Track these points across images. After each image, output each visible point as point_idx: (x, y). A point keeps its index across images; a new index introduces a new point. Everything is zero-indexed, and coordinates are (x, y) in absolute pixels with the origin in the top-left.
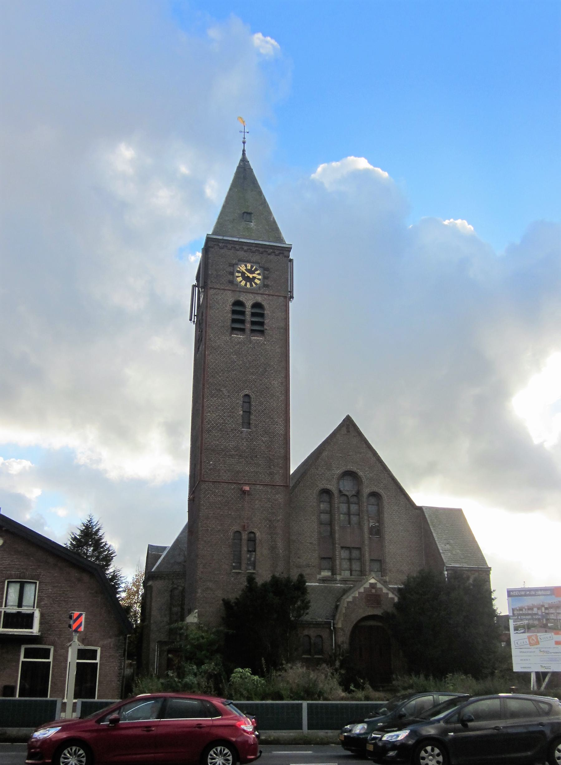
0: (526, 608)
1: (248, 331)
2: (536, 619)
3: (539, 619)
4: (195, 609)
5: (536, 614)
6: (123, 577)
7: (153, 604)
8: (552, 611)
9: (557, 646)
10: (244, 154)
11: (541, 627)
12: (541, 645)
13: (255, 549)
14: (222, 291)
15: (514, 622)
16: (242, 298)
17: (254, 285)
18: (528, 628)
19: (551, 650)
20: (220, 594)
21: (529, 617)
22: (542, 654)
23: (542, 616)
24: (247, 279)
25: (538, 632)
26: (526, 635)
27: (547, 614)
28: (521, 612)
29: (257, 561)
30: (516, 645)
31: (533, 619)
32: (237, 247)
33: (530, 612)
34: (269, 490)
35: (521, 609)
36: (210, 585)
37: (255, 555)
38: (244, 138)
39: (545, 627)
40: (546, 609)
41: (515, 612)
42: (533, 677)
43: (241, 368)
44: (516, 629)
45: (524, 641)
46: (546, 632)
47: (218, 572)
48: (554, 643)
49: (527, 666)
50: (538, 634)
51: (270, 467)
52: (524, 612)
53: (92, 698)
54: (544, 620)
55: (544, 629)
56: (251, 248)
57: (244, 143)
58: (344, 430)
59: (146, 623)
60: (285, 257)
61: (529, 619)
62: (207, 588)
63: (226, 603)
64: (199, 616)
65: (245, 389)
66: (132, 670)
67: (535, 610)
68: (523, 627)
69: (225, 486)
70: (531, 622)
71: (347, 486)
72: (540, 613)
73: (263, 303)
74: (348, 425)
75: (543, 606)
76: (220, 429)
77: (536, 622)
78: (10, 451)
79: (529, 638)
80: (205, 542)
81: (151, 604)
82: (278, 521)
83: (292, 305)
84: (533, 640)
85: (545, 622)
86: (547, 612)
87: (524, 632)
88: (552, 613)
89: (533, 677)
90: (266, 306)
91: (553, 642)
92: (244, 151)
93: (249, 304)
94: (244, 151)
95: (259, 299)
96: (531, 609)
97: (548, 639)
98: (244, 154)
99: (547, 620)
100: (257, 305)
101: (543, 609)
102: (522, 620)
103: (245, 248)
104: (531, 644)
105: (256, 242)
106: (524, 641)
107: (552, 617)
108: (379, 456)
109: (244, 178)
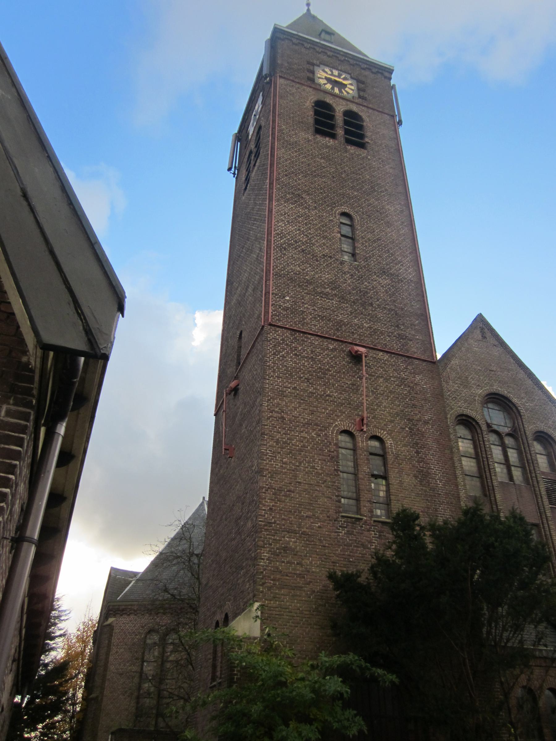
4: (255, 598)
6: (65, 611)
7: (111, 658)
13: (386, 470)
14: (298, 86)
17: (345, 93)
20: (317, 570)
29: (392, 497)
34: (403, 366)
36: (292, 541)
37: (388, 485)
43: (333, 177)
47: (310, 513)
51: (397, 326)
58: (478, 334)
59: (93, 696)
60: (385, 77)
62: (285, 549)
63: (344, 583)
64: (265, 620)
65: (342, 205)
66: (388, 556)
69: (317, 342)
71: (497, 418)
74: (482, 329)
76: (303, 251)
80: (277, 442)
81: (107, 659)
82: (426, 423)
83: (402, 130)
95: (355, 108)
108: (537, 378)
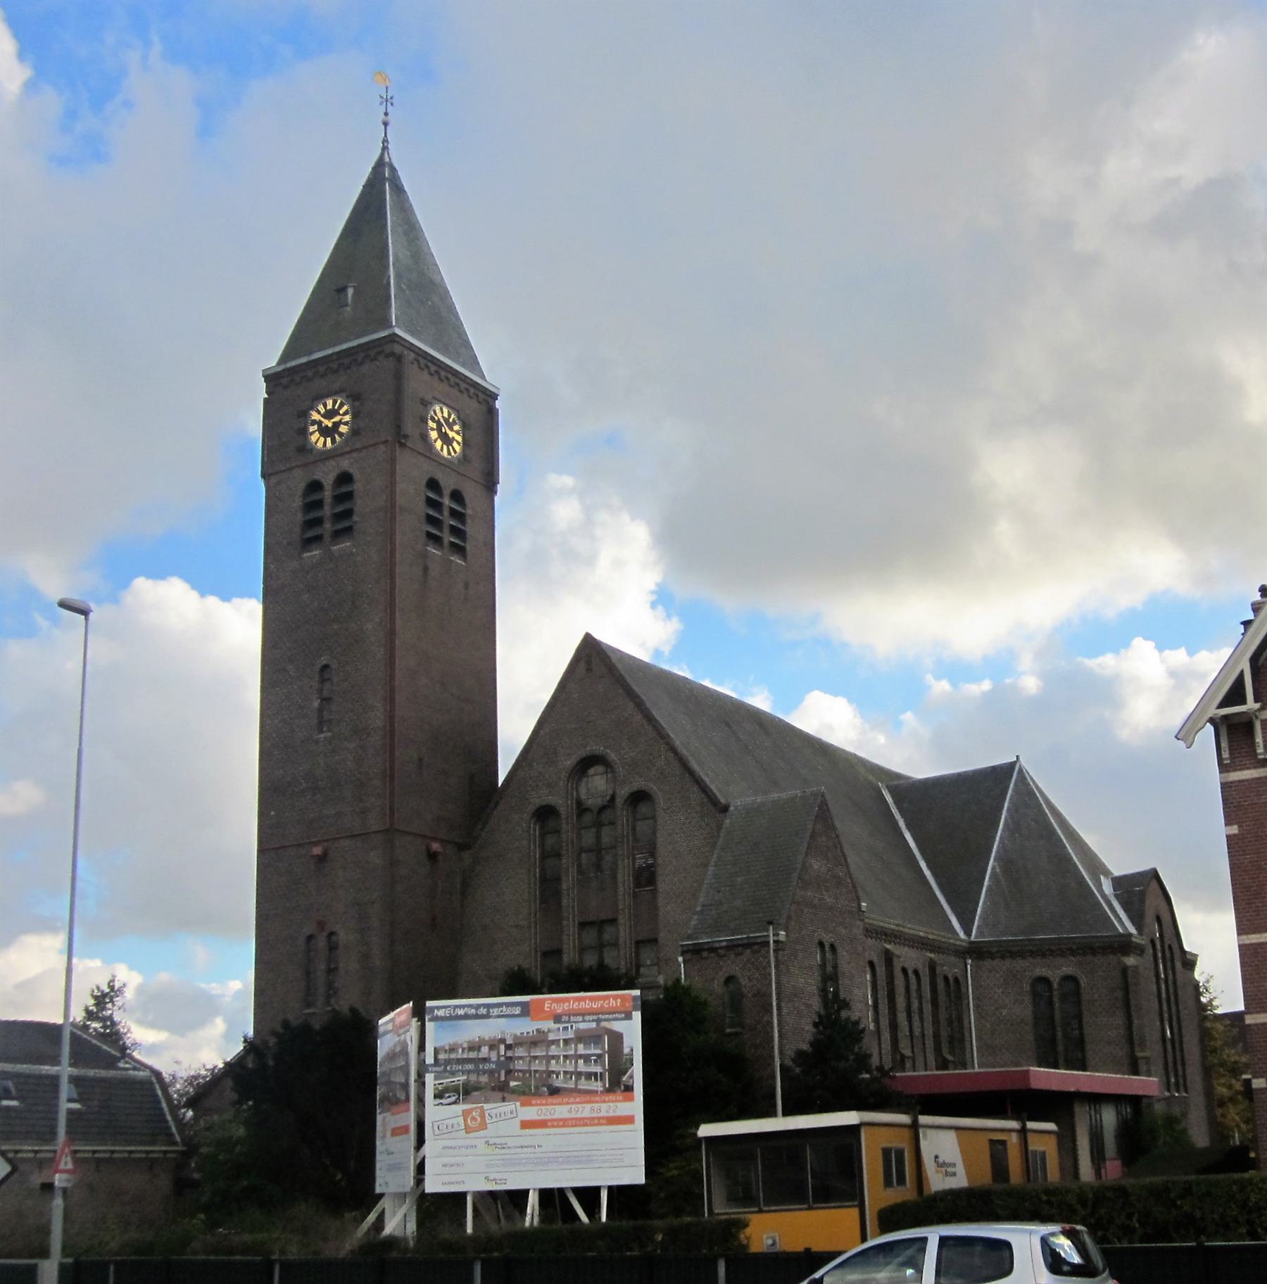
0: (465, 1045)
2: (484, 1072)
3: (491, 1072)
5: (485, 1060)
8: (520, 1052)
9: (528, 1131)
10: (385, 148)
11: (493, 1089)
12: (491, 1130)
15: (436, 1079)
16: (318, 476)
18: (466, 1092)
19: (510, 1142)
21: (470, 1067)
22: (489, 1150)
23: (498, 1063)
24: (325, 432)
25: (487, 1101)
27: (510, 1059)
28: (453, 1056)
30: (437, 1132)
31: (477, 1072)
32: (310, 374)
33: (473, 1055)
35: (452, 1049)
38: (386, 114)
39: (502, 1090)
40: (508, 1047)
41: (442, 1056)
44: (439, 1095)
45: (454, 1121)
46: (504, 1100)
48: (518, 1124)
49: (454, 1178)
50: (486, 1106)
52: (460, 1054)
54: (503, 1073)
55: (500, 1095)
56: (331, 365)
57: (386, 124)
61: (469, 1072)
67: (485, 1050)
68: (455, 1090)
70: (473, 1078)
72: (494, 1056)
73: (351, 471)
75: (503, 1041)
77: (484, 1079)
78: (6, 1075)
79: (466, 1114)
84: (474, 1119)
85: (503, 1078)
86: (509, 1054)
87: (455, 1103)
88: (521, 1058)
90: (356, 474)
91: (517, 1123)
92: (385, 141)
93: (328, 481)
94: (385, 141)
96: (474, 1047)
97: (505, 1116)
99: (509, 1072)
101: (502, 1047)
102: (453, 1073)
103: (322, 369)
104: (468, 1130)
105: (337, 349)
106: (454, 1121)
107: (519, 1065)
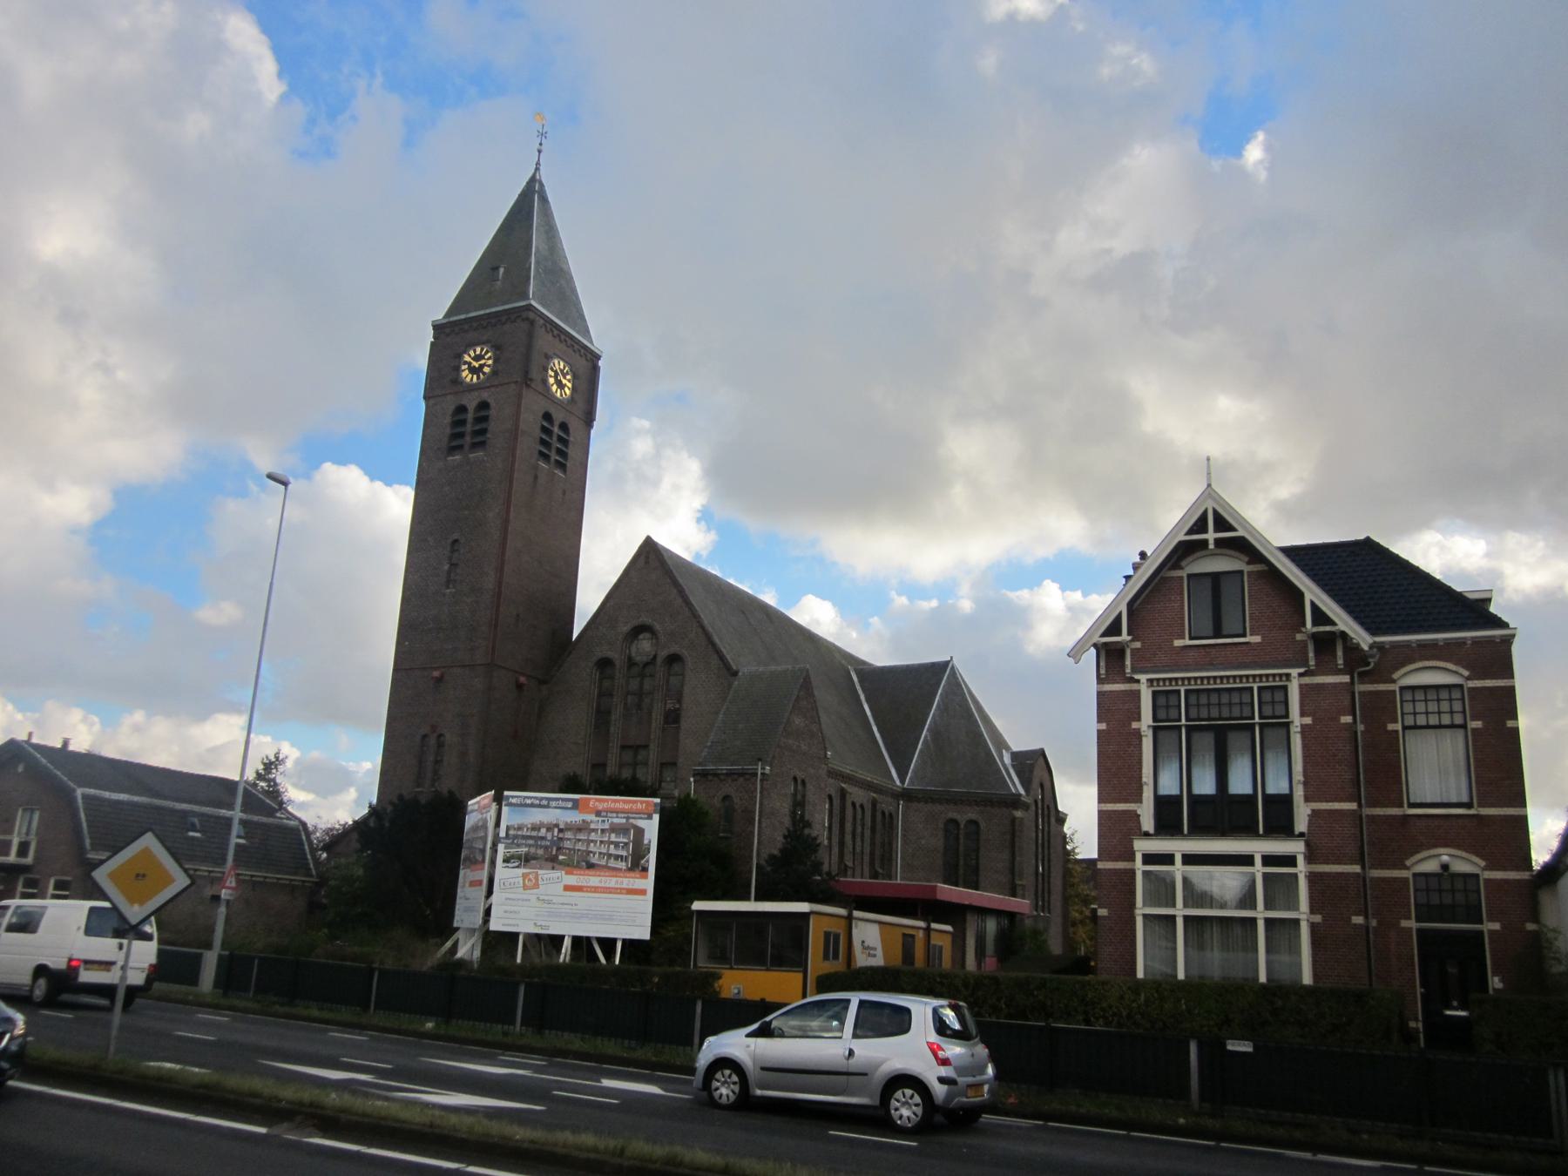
1: (466, 448)
3: (546, 848)
5: (543, 838)
8: (569, 835)
10: (537, 169)
18: (526, 860)
23: (552, 841)
26: (520, 871)
31: (537, 846)
33: (534, 834)
35: (520, 828)
39: (552, 861)
40: (561, 831)
42: (567, 943)
52: (525, 832)
53: (1289, 909)
67: (543, 831)
68: (519, 858)
70: (533, 850)
75: (557, 825)
77: (540, 852)
79: (524, 876)
89: (567, 943)
92: (538, 164)
94: (538, 164)
96: (535, 828)
97: (554, 880)
98: (537, 169)
99: (559, 849)
100: (484, 405)
102: (518, 846)
104: (525, 887)
107: (567, 844)
109: (529, 207)
